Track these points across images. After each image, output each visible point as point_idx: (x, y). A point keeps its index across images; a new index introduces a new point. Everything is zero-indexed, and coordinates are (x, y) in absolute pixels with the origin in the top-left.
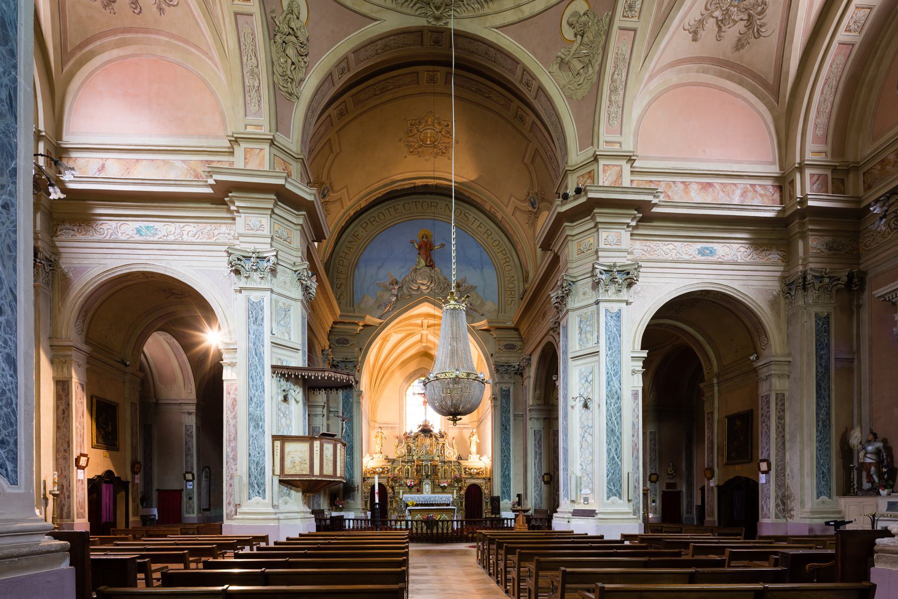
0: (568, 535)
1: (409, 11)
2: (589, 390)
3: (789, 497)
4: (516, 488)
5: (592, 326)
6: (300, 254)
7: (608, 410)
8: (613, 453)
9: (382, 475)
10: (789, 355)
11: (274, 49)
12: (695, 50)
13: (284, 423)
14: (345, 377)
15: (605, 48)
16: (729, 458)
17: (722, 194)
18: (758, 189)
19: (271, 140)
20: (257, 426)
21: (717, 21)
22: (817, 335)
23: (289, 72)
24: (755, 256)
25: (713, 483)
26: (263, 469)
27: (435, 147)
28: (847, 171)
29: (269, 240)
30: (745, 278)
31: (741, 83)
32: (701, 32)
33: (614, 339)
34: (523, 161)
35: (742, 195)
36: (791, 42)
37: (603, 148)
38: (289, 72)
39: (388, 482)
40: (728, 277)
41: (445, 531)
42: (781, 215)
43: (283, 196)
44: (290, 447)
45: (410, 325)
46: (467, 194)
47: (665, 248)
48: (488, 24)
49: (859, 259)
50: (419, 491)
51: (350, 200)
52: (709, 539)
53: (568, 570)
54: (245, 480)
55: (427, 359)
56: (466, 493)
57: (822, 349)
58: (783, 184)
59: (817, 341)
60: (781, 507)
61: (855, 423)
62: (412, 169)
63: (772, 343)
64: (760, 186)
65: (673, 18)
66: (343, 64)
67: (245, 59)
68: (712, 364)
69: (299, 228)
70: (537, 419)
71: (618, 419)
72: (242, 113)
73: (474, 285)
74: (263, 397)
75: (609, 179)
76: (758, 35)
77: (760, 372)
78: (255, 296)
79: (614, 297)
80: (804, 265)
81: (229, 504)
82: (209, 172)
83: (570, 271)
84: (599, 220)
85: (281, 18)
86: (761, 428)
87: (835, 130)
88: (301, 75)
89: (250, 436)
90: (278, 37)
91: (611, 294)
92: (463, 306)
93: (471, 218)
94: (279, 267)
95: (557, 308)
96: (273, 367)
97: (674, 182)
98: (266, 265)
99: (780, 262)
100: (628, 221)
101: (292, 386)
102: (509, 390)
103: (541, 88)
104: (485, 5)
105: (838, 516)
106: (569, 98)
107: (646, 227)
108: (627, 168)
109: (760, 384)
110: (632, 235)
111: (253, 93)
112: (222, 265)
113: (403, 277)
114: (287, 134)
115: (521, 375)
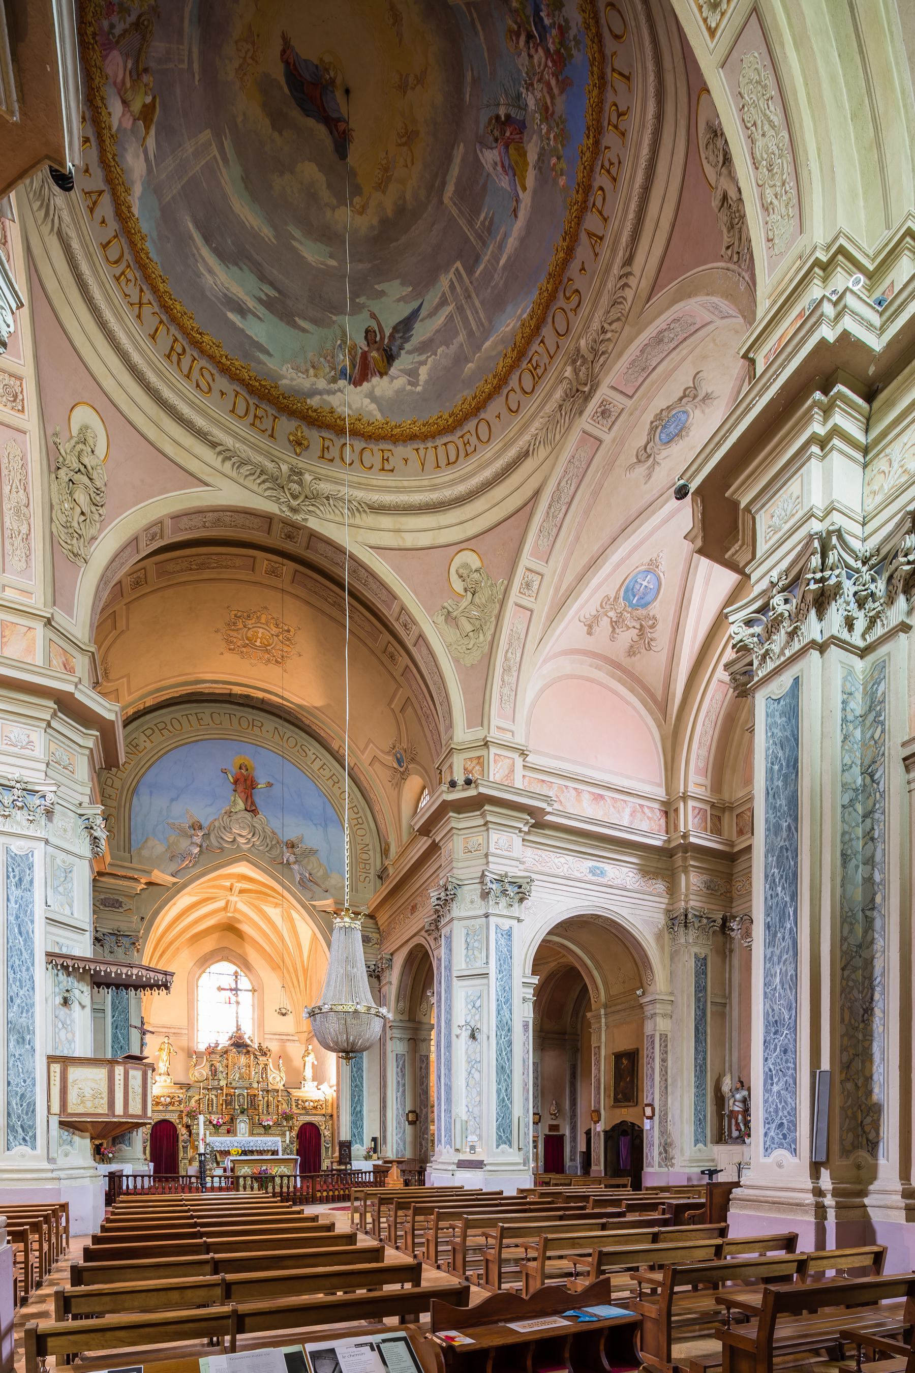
0: (457, 1193)
1: (255, 487)
2: (477, 1017)
3: (671, 1145)
4: (370, 1129)
5: (479, 941)
6: (88, 791)
7: (498, 1043)
8: (503, 1093)
9: (171, 1108)
10: (671, 993)
11: (54, 486)
12: (588, 643)
13: (63, 1038)
15: (499, 617)
16: (616, 1100)
17: (612, 809)
18: (646, 810)
20: (21, 1041)
21: (611, 622)
22: (696, 977)
23: (75, 524)
24: (643, 884)
25: (600, 1127)
28: (723, 810)
29: (43, 767)
30: (633, 906)
31: (632, 691)
32: (595, 627)
33: (504, 961)
35: (631, 815)
36: (678, 665)
37: (494, 735)
38: (75, 524)
39: (181, 1118)
40: (618, 903)
41: (285, 1189)
42: (666, 846)
43: (66, 705)
44: (74, 1073)
45: (214, 887)
46: (307, 722)
47: (556, 860)
48: (360, 539)
49: (732, 902)
51: (130, 694)
52: (595, 1190)
53: (506, 1225)
55: (232, 936)
56: (298, 1136)
57: (700, 991)
58: (669, 810)
59: (696, 982)
60: (664, 1155)
61: (727, 1069)
62: (224, 668)
63: (657, 980)
64: (648, 807)
65: (570, 608)
66: (155, 528)
68: (599, 994)
69: (87, 752)
70: (400, 1039)
73: (315, 847)
75: (500, 774)
76: (649, 648)
77: (646, 1008)
78: (18, 846)
80: (686, 902)
83: (455, 871)
84: (489, 818)
85: (69, 446)
86: (645, 1070)
87: (717, 748)
88: (93, 532)
89: (10, 1055)
90: (62, 473)
91: (502, 908)
93: (310, 753)
96: (48, 954)
97: (566, 787)
98: (38, 802)
99: (665, 894)
100: (521, 825)
103: (421, 637)
104: (357, 514)
105: (712, 1164)
106: (456, 661)
108: (519, 762)
109: (646, 1022)
110: (523, 840)
111: (18, 541)
113: (211, 819)
114: (69, 611)
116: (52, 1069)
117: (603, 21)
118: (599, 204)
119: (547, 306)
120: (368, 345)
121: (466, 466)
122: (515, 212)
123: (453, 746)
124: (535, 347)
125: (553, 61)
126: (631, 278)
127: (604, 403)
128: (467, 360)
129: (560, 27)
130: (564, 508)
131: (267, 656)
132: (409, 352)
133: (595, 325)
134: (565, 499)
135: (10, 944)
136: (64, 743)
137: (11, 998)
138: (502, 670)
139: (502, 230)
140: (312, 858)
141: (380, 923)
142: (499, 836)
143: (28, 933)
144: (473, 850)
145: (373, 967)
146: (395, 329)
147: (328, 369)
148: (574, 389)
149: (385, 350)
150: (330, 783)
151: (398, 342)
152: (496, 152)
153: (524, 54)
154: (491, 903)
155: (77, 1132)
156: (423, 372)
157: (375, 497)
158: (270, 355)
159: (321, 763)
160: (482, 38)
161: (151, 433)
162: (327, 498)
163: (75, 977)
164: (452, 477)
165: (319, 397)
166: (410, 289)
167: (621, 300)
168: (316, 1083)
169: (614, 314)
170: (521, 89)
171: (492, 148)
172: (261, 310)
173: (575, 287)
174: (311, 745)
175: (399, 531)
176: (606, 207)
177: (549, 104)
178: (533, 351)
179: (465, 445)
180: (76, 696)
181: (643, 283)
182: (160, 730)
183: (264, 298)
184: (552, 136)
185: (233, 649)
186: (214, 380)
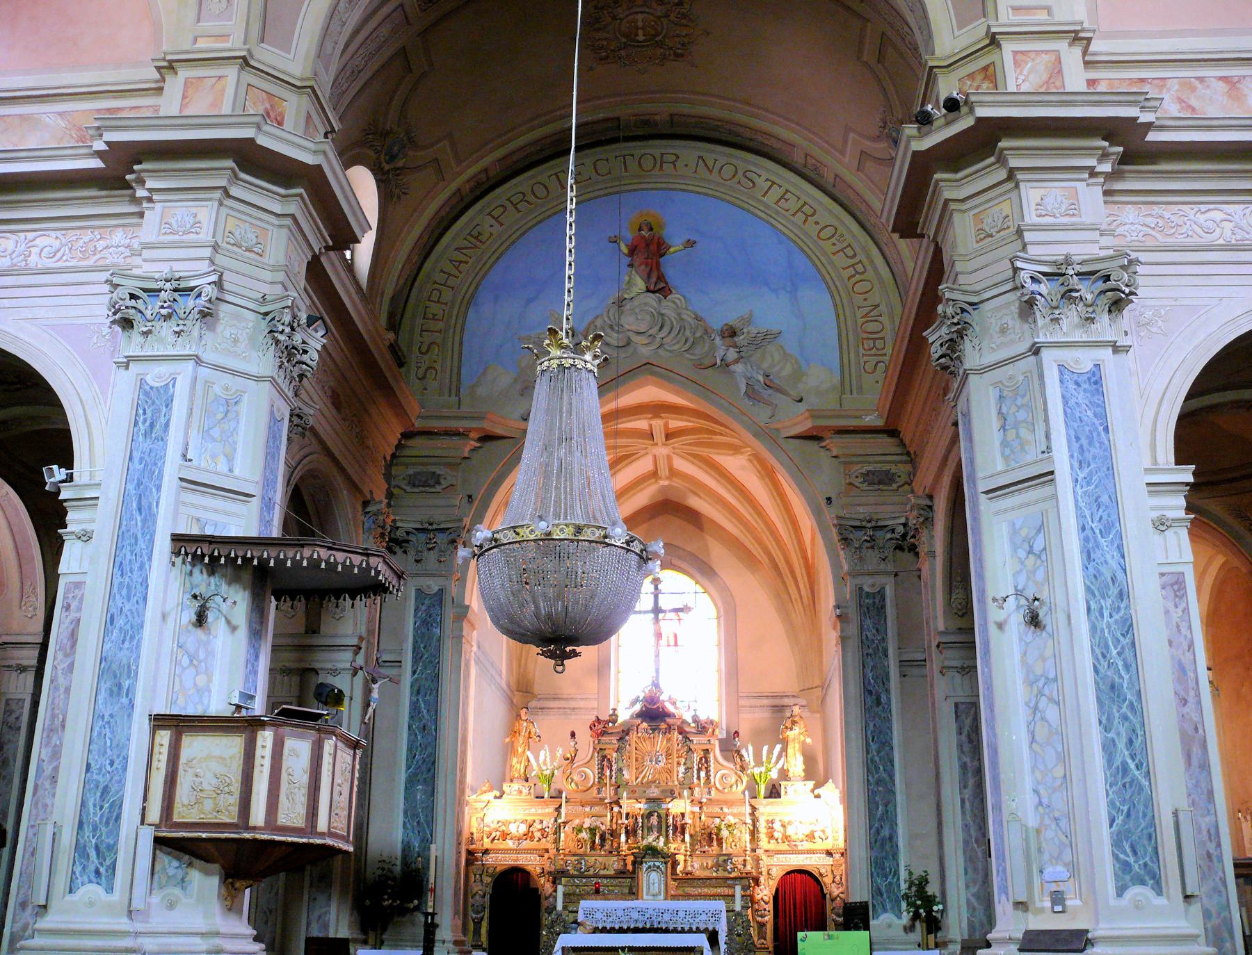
2: (1040, 575)
5: (1028, 407)
7: (1093, 629)
8: (1122, 752)
9: (526, 844)
14: (357, 559)
19: (244, 58)
26: (118, 806)
27: (659, 45)
29: (207, 252)
44: (195, 746)
47: (1201, 218)
50: (633, 893)
54: (67, 837)
55: (676, 523)
71: (1128, 654)
72: (191, 14)
73: (775, 330)
74: (140, 614)
75: (1025, 81)
78: (156, 374)
79: (1079, 336)
81: (23, 905)
82: (98, 128)
84: (1013, 163)
89: (97, 716)
91: (1070, 324)
93: (760, 181)
94: (224, 307)
95: (945, 368)
96: (177, 539)
100: (1091, 162)
101: (224, 587)
102: (881, 594)
107: (1141, 175)
108: (1072, 57)
110: (1106, 193)
112: (95, 309)
113: (590, 318)
115: (913, 549)
116: (158, 740)
123: (931, 64)
135: (123, 527)
136: (251, 216)
137: (112, 616)
140: (771, 348)
141: (907, 442)
142: (1042, 191)
143: (150, 507)
144: (993, 231)
145: (900, 529)
154: (1040, 322)
155: (197, 862)
163: (224, 576)
168: (811, 784)
174: (762, 167)
180: (259, 142)
182: (515, 205)
185: (607, 58)
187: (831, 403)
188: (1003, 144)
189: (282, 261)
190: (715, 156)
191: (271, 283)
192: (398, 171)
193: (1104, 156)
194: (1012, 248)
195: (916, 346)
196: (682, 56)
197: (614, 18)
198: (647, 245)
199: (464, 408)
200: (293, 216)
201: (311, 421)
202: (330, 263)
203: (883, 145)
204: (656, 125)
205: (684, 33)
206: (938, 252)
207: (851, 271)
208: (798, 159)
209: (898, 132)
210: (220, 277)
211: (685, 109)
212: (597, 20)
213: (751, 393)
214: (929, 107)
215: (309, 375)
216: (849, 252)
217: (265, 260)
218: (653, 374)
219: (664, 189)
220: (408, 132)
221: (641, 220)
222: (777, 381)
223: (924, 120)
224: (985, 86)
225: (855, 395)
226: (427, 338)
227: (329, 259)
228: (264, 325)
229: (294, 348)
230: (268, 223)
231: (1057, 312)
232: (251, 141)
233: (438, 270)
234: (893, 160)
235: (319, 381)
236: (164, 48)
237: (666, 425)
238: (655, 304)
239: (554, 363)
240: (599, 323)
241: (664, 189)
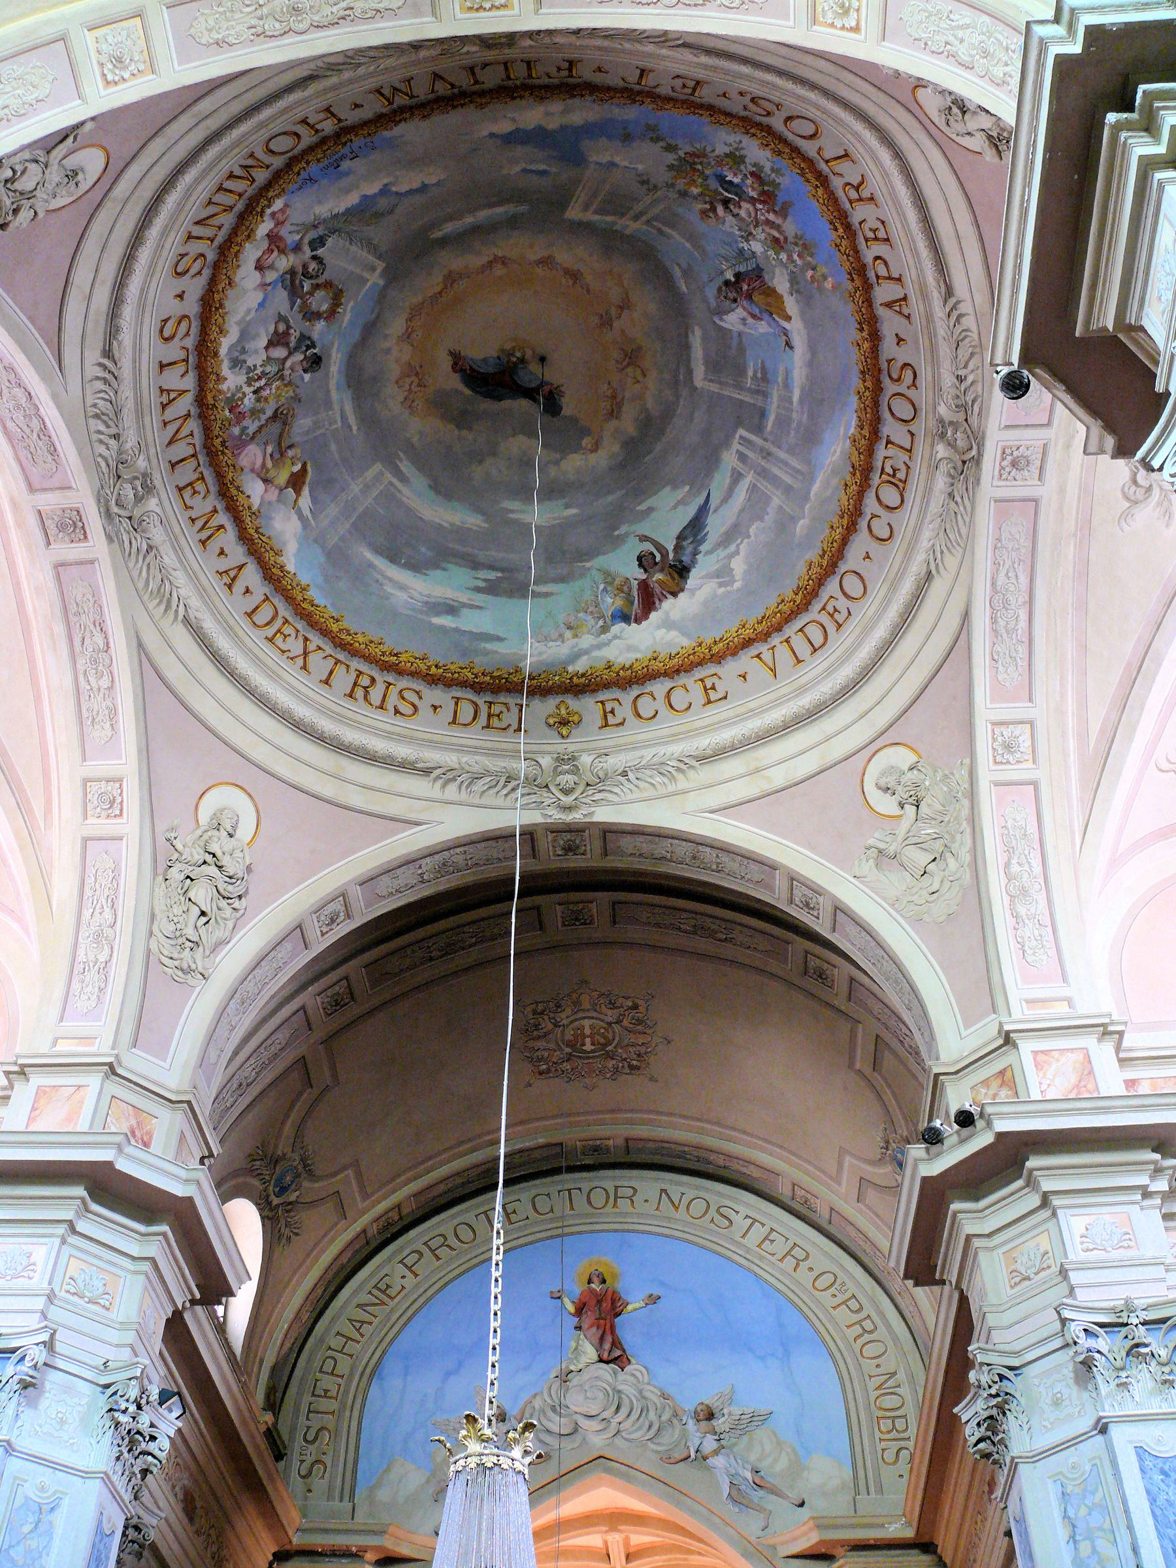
1: (500, 801)
11: (160, 891)
15: (973, 819)
19: (111, 1065)
27: (610, 1056)
29: (40, 1303)
34: (851, 1065)
37: (1018, 1015)
43: (108, 1188)
67: (87, 914)
72: (55, 1013)
73: (763, 1409)
75: (1049, 1088)
79: (1156, 1406)
84: (1047, 1185)
88: (220, 934)
92: (517, 1458)
94: (53, 1376)
95: (987, 1456)
100: (1143, 1180)
103: (839, 909)
104: (679, 776)
106: (917, 921)
108: (1103, 1054)
111: (92, 976)
113: (525, 1397)
117: (791, 137)
118: (882, 271)
119: (876, 404)
120: (646, 571)
121: (840, 642)
122: (788, 344)
123: (936, 1070)
124: (881, 452)
125: (762, 202)
126: (961, 305)
127: (1008, 451)
128: (794, 519)
129: (752, 174)
130: (1023, 616)
131: (611, 1064)
132: (708, 553)
133: (948, 380)
134: (1018, 599)
136: (100, 1258)
138: (1006, 899)
139: (781, 369)
140: (761, 1434)
142: (1086, 1220)
144: (1030, 1273)
146: (680, 537)
147: (592, 622)
148: (960, 464)
149: (671, 566)
150: (790, 1262)
151: (689, 550)
152: (740, 310)
153: (729, 218)
154: (1104, 1389)
156: (738, 565)
157: (704, 743)
158: (499, 639)
159: (764, 1231)
160: (677, 237)
161: (328, 789)
162: (624, 774)
164: (825, 664)
165: (586, 657)
166: (687, 488)
167: (964, 334)
169: (963, 353)
170: (741, 245)
171: (733, 310)
172: (480, 599)
173: (900, 364)
175: (758, 771)
176: (891, 269)
177: (777, 235)
178: (882, 459)
179: (832, 616)
181: (978, 299)
183: (482, 584)
184: (795, 257)
185: (548, 1071)
186: (420, 698)
187: (840, 1507)
188: (1032, 1162)
189: (134, 1316)
190: (683, 1190)
191: (117, 1346)
192: (290, 1206)
193: (1158, 1171)
194: (1057, 1294)
195: (946, 1428)
196: (638, 1068)
197: (556, 1025)
198: (599, 1302)
199: (360, 1517)
200: (153, 1260)
201: (152, 1535)
202: (197, 1323)
203: (888, 1169)
204: (608, 1150)
205: (640, 1041)
206: (964, 1301)
207: (857, 1329)
208: (784, 1191)
209: (903, 1153)
210: (52, 1336)
211: (642, 1131)
212: (537, 1026)
213: (737, 1497)
214: (937, 1123)
215: (155, 1470)
216: (853, 1304)
217: (113, 1315)
218: (608, 1471)
219: (616, 1231)
220: (303, 1160)
221: (592, 1270)
222: (770, 1480)
223: (933, 1138)
224: (1004, 1094)
225: (873, 1495)
226: (316, 1422)
227: (195, 1316)
228: (103, 1403)
229: (138, 1432)
230: (121, 1268)
231: (1124, 1374)
232: (109, 1165)
233: (334, 1332)
234: (899, 1186)
235: (168, 1478)
236: (17, 1050)
237: (627, 1541)
238: (610, 1379)
239: (473, 1462)
240: (537, 1403)
241: (616, 1231)
